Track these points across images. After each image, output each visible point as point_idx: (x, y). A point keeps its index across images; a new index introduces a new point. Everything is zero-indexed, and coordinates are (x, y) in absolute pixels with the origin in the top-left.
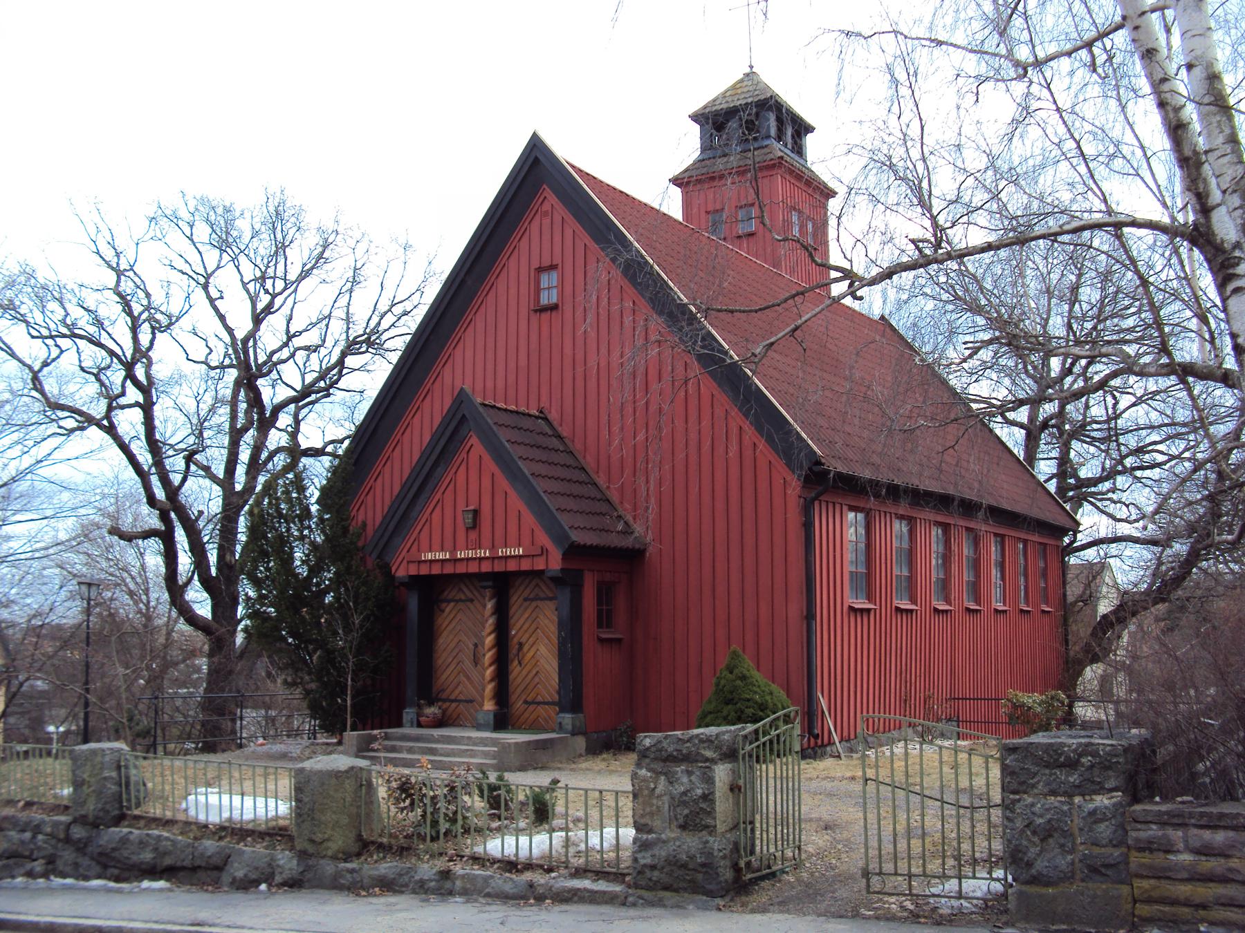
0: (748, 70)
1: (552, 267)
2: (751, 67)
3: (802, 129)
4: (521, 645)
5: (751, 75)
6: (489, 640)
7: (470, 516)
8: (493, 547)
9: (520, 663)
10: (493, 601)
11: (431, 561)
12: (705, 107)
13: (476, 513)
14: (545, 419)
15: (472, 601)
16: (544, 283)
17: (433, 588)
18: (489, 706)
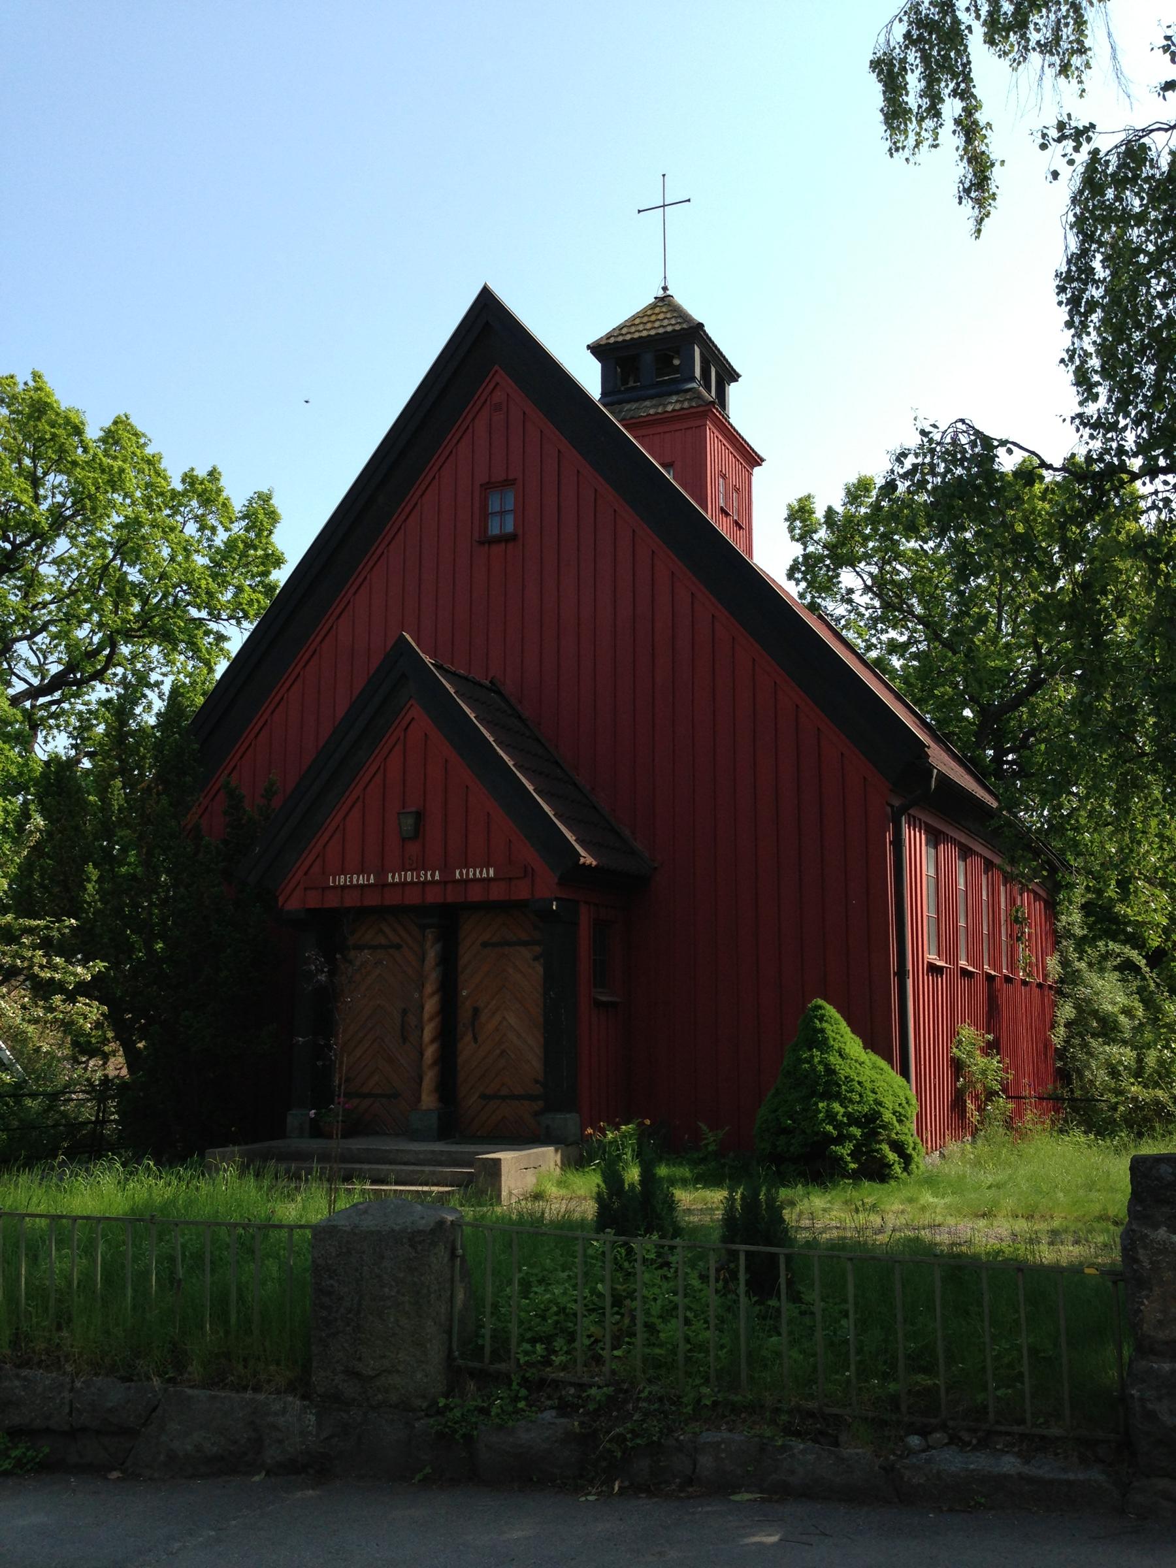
0: (661, 293)
1: (508, 483)
2: (665, 289)
3: (729, 375)
4: (476, 1011)
5: (664, 302)
6: (431, 1005)
7: (410, 821)
8: (447, 869)
9: (475, 1039)
10: (438, 947)
11: (344, 887)
12: (609, 336)
13: (419, 816)
14: (498, 693)
15: (398, 947)
16: (494, 504)
17: (332, 926)
18: (428, 1100)
